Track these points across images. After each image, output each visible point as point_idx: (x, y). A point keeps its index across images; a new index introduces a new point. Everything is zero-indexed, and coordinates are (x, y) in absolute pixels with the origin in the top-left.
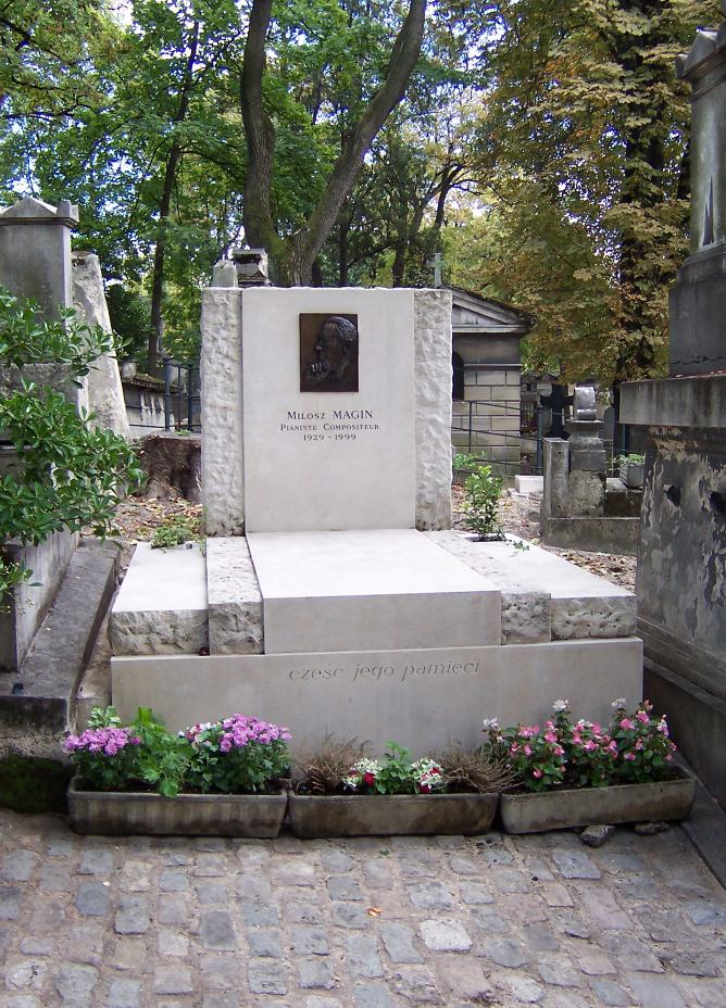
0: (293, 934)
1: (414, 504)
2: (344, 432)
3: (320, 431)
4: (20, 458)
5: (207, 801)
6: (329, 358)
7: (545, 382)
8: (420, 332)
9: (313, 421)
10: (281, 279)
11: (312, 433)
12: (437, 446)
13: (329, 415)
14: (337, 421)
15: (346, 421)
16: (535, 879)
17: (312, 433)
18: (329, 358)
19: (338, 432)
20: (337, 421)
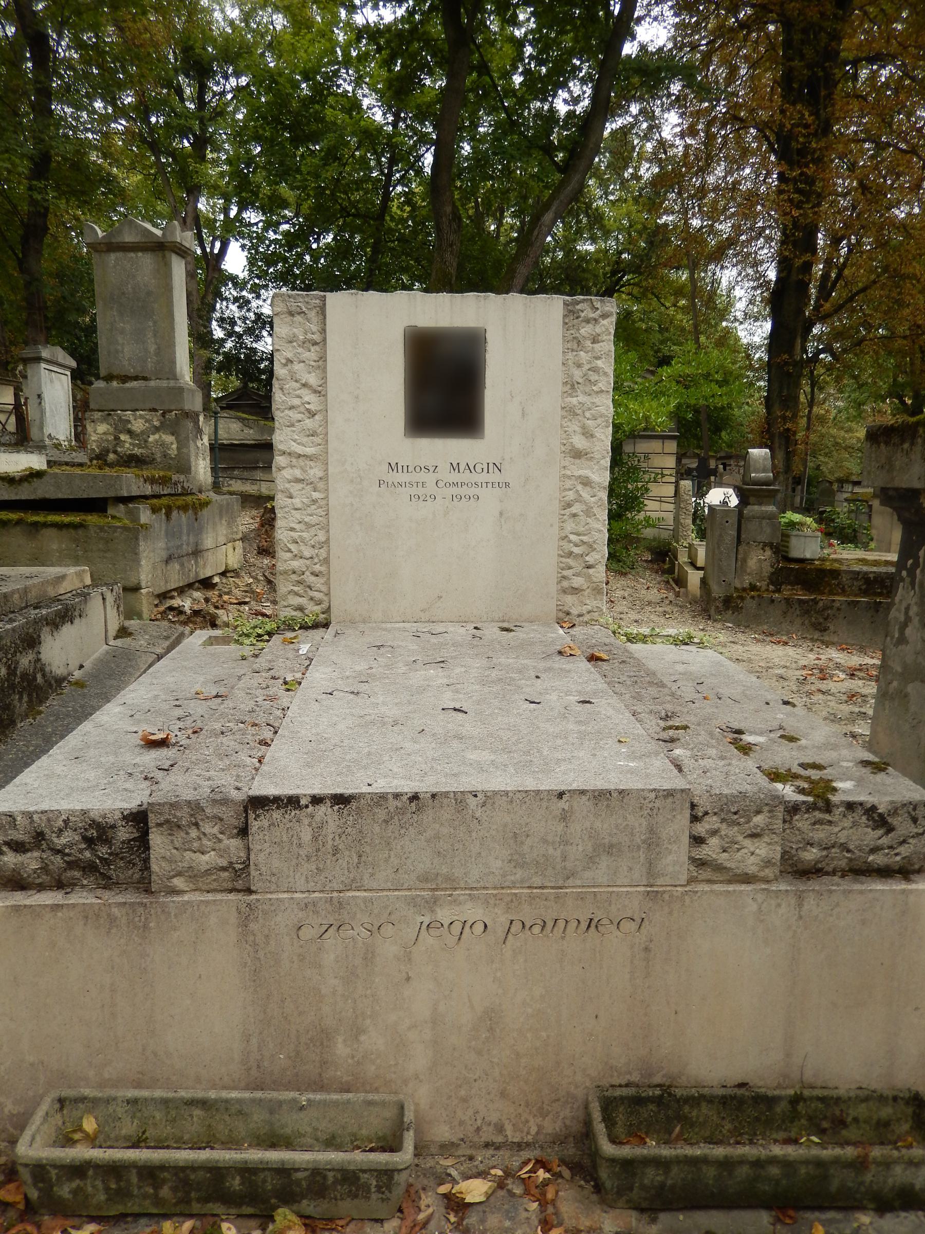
0: (238, 776)
1: (553, 588)
2: (464, 491)
3: (431, 488)
4: (64, 821)
5: (92, 1140)
6: (445, 391)
7: (689, 457)
8: (570, 356)
9: (422, 476)
10: (376, 279)
11: (420, 491)
12: (588, 512)
13: (444, 467)
14: (455, 477)
15: (466, 477)
16: (917, 1009)
17: (420, 491)
18: (445, 391)
19: (455, 491)
20: (455, 477)
